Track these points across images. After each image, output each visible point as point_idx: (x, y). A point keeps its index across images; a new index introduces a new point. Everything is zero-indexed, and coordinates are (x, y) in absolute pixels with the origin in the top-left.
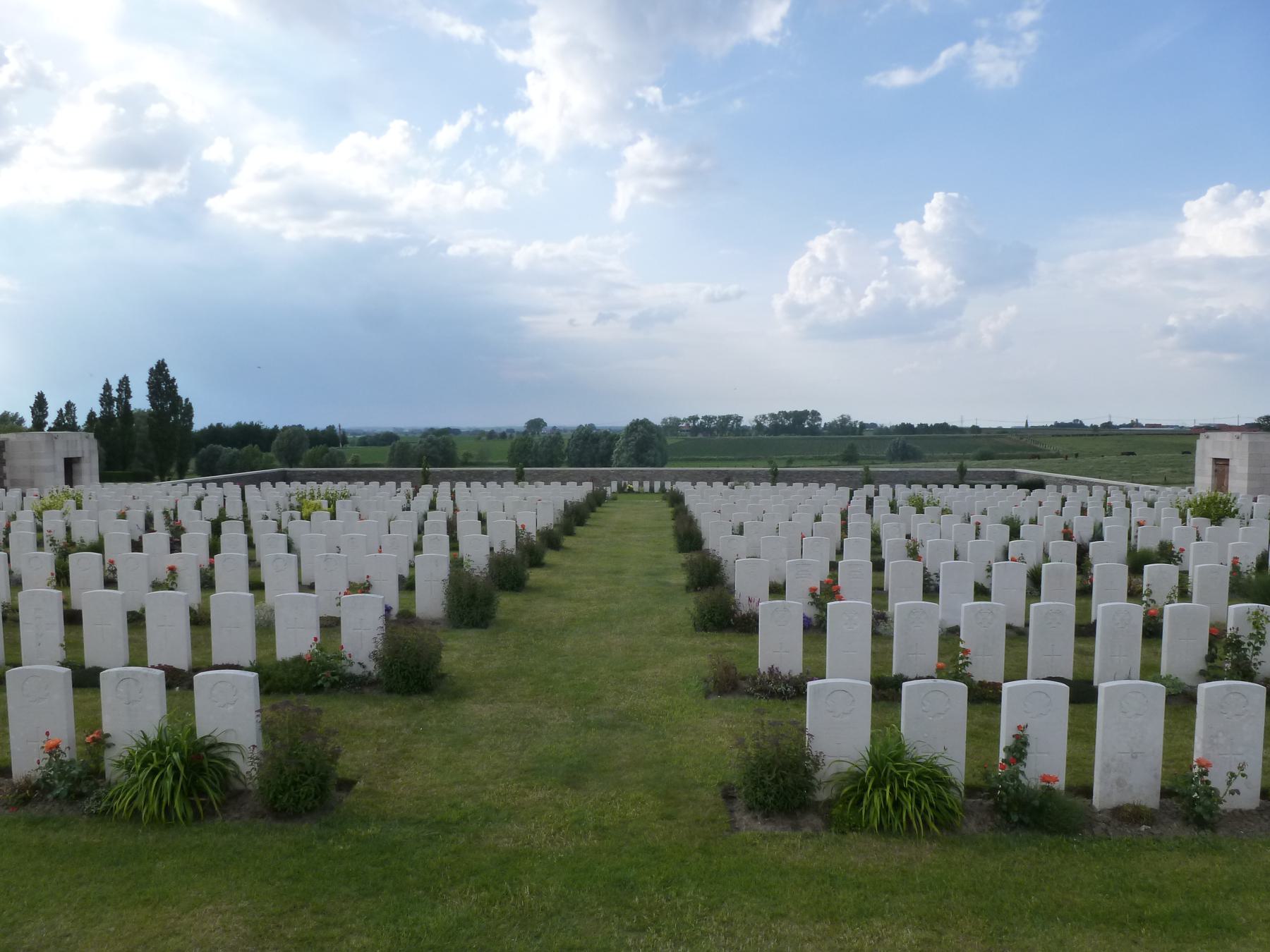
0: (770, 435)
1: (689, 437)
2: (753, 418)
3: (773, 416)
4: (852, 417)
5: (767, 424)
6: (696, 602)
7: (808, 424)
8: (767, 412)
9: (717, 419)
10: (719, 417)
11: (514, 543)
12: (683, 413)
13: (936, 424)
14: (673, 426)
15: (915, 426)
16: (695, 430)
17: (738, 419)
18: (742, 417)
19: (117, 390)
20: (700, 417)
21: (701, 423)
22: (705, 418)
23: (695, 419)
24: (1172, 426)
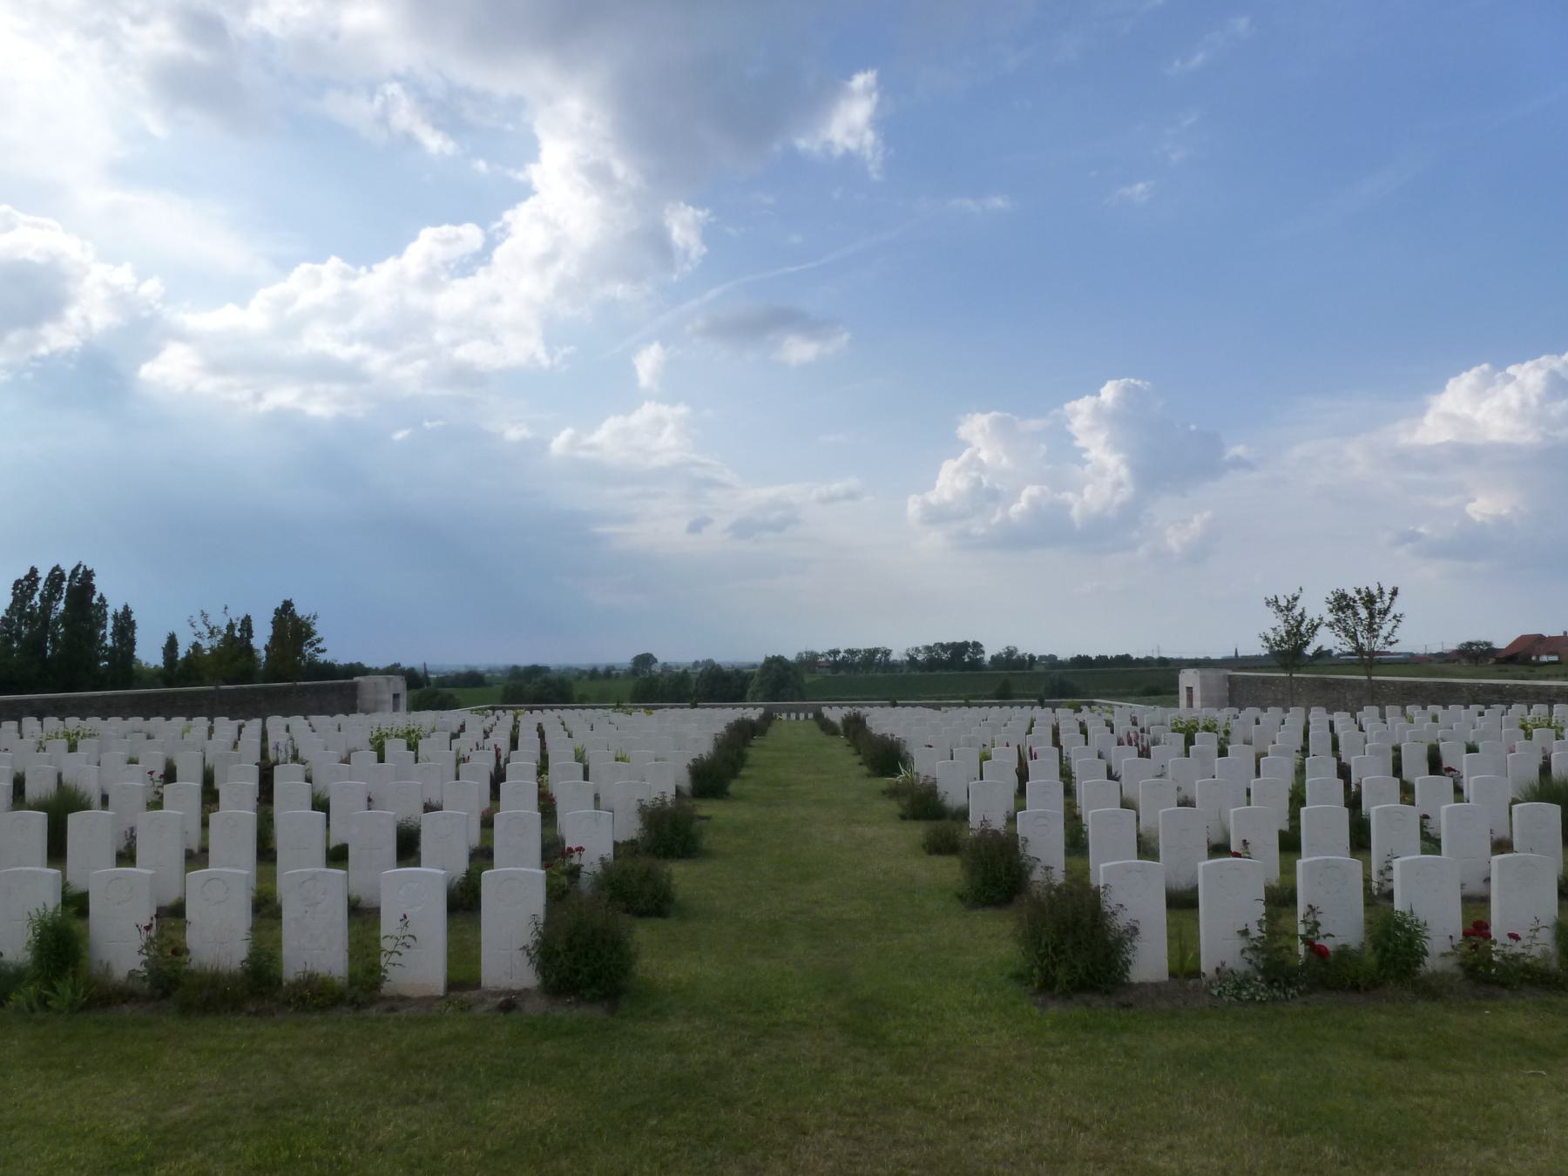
0: (923, 671)
1: (829, 674)
2: (904, 651)
3: (928, 649)
4: (1019, 648)
5: (920, 657)
6: (1545, 953)
7: (969, 657)
8: (921, 644)
9: (862, 653)
10: (865, 651)
11: (914, 824)
12: (821, 646)
13: (1137, 659)
14: (810, 662)
15: (1094, 658)
16: (836, 666)
17: (887, 653)
18: (891, 651)
19: (239, 630)
20: (842, 650)
21: (844, 657)
22: (849, 651)
23: (835, 652)
24: (1400, 654)
